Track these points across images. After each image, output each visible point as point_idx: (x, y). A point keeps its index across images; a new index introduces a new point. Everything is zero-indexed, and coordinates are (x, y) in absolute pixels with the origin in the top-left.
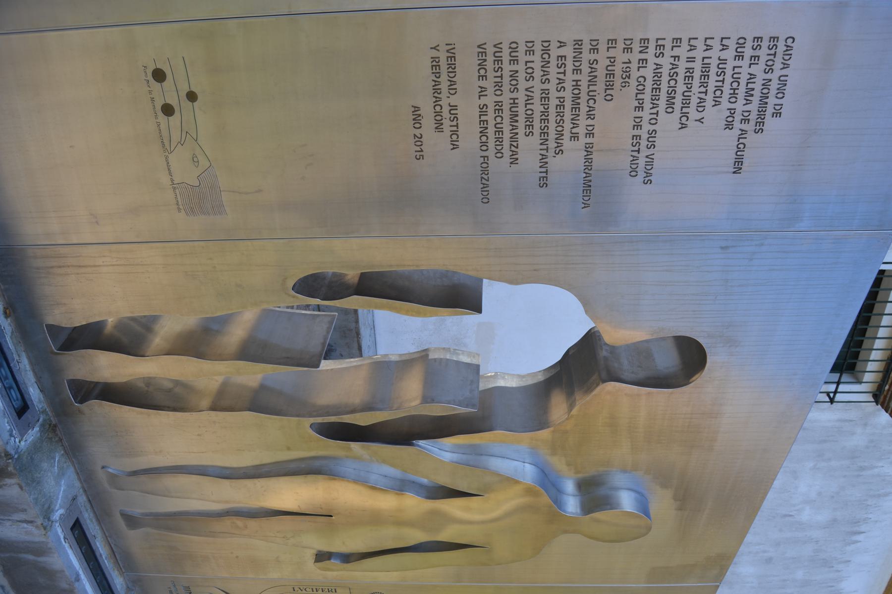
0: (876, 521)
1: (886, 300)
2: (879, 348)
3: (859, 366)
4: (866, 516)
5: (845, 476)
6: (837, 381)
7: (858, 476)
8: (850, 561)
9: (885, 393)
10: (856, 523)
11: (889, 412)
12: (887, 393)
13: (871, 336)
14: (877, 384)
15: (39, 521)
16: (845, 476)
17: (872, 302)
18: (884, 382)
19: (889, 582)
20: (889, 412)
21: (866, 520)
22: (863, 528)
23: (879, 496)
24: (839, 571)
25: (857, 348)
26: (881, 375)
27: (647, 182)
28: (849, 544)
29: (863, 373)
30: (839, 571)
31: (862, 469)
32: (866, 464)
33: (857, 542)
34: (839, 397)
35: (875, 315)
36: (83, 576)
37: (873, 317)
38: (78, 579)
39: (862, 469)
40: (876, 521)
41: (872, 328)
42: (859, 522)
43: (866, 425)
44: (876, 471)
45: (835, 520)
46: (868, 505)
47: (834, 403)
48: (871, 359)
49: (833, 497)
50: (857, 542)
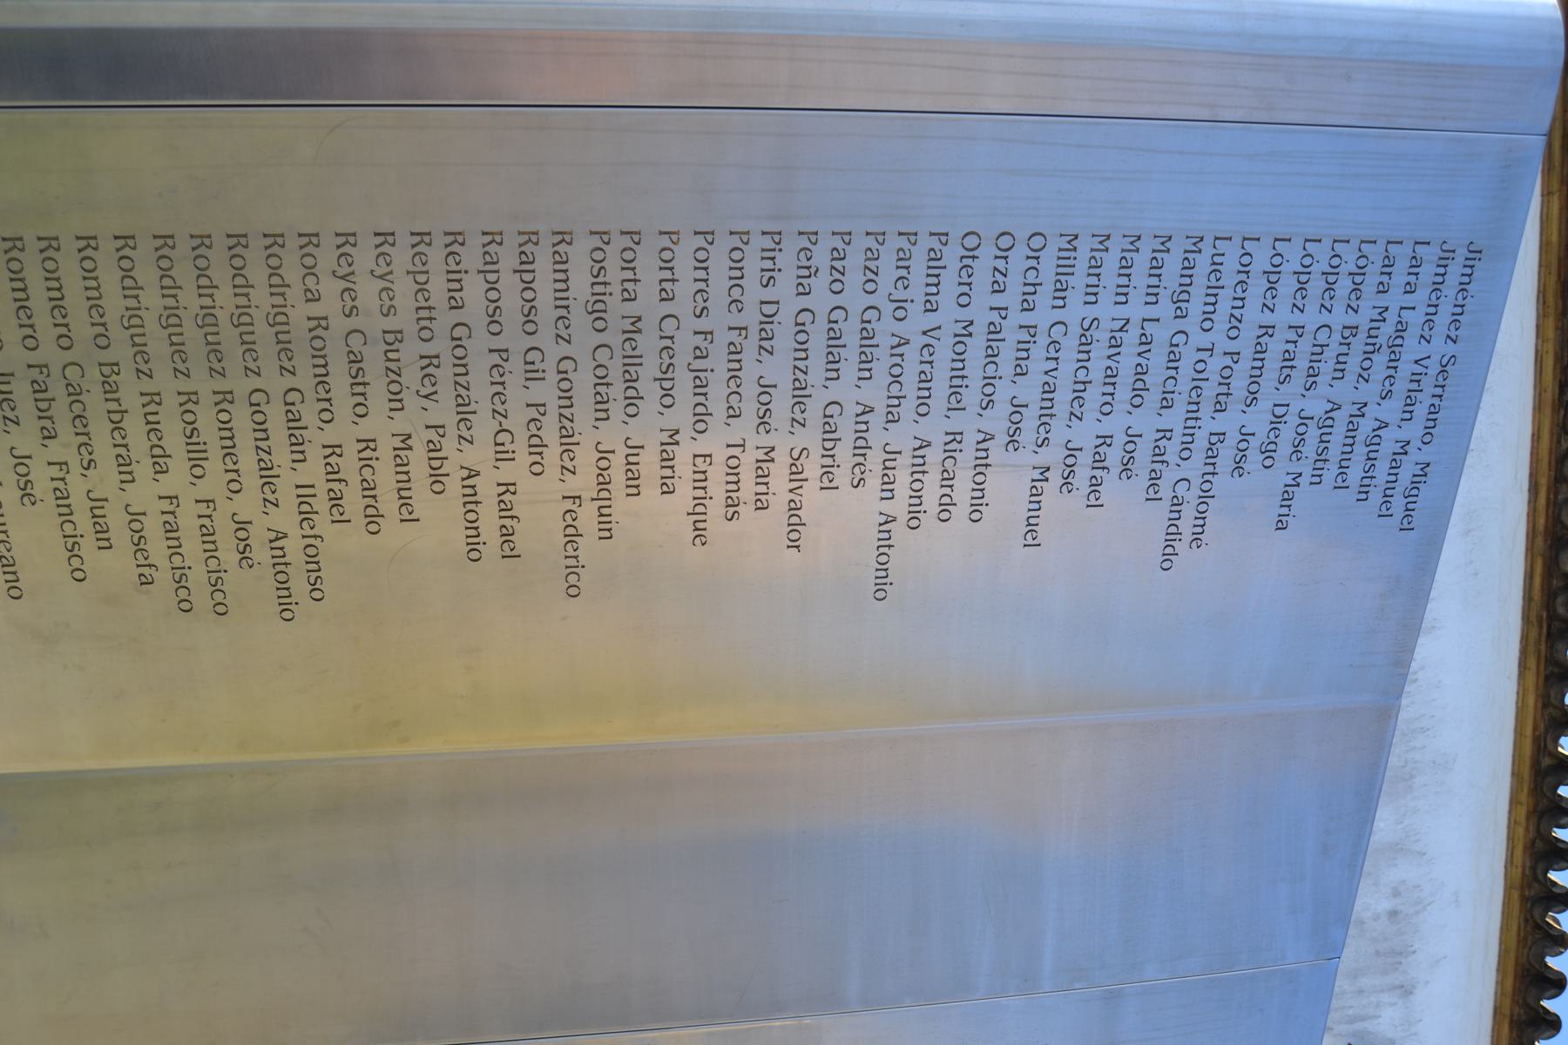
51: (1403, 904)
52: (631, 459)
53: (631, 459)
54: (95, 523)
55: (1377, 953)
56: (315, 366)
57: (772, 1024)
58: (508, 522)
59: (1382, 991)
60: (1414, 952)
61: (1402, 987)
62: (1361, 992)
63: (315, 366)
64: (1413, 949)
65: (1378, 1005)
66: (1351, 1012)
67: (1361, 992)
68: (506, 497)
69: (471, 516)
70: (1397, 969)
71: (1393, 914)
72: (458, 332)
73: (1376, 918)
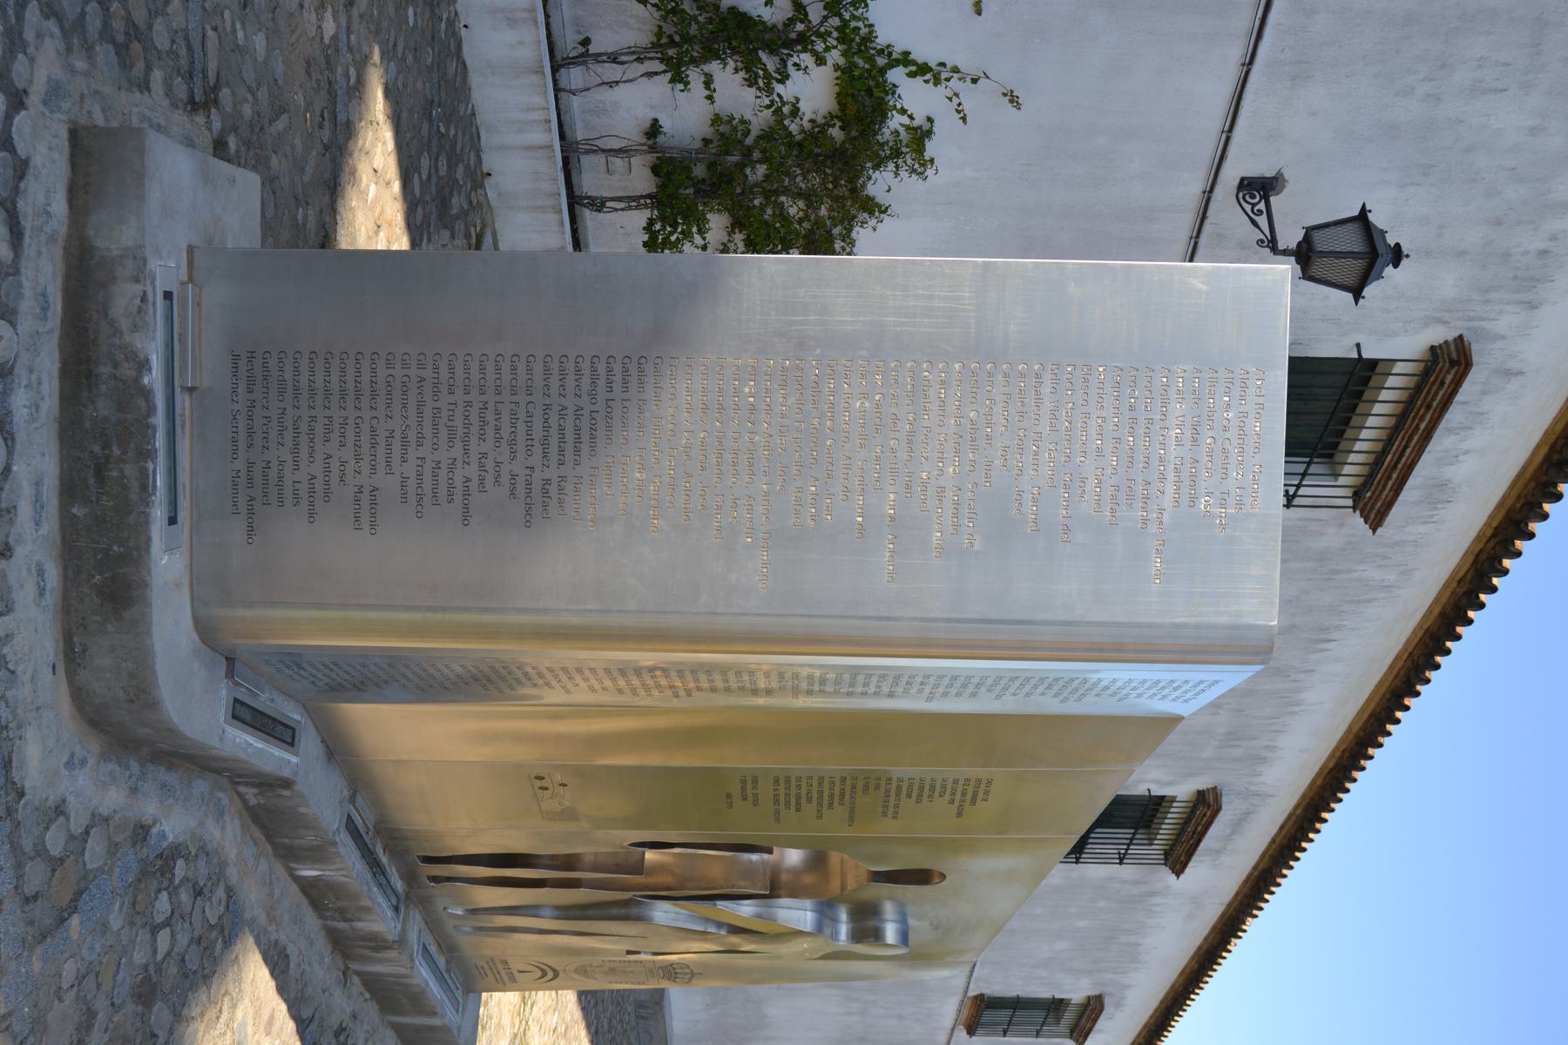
0: (1354, 629)
1: (1344, 461)
2: (1355, 462)
3: (1338, 457)
4: (1339, 623)
5: (1309, 580)
6: (1302, 471)
7: (1329, 580)
8: (1313, 671)
9: (1366, 500)
10: (1323, 630)
11: (1370, 522)
12: (1368, 502)
13: (1344, 449)
14: (1388, 431)
15: (409, 966)
16: (1309, 580)
17: (1366, 374)
18: (1365, 487)
19: (1371, 694)
20: (1370, 522)
21: (1338, 628)
22: (1334, 635)
23: (1359, 602)
24: (1298, 681)
25: (1332, 449)
26: (1421, 366)
27: (895, 817)
28: (1314, 652)
29: (1340, 466)
30: (1298, 681)
31: (1334, 572)
32: (1340, 567)
33: (1325, 650)
34: (1297, 501)
35: (1353, 427)
36: (430, 983)
37: (1354, 418)
38: (427, 985)
39: (1334, 572)
40: (1354, 629)
41: (1379, 376)
42: (1328, 629)
43: (1341, 525)
44: (1355, 575)
45: (1293, 627)
46: (1342, 612)
47: (1292, 508)
48: (1366, 425)
49: (1291, 601)
50: (1325, 650)
51: (1557, 246)
52: (404, 484)
53: (404, 484)
54: (624, 379)
55: (1516, 278)
56: (403, 399)
57: (370, 954)
58: (482, 473)
59: (1508, 303)
60: (1553, 281)
61: (1530, 303)
62: (1488, 301)
63: (403, 399)
64: (1552, 278)
65: (1500, 312)
66: (1472, 314)
67: (1488, 301)
68: (483, 460)
69: (373, 511)
70: (1529, 290)
71: (1544, 253)
72: (390, 379)
73: (1526, 253)
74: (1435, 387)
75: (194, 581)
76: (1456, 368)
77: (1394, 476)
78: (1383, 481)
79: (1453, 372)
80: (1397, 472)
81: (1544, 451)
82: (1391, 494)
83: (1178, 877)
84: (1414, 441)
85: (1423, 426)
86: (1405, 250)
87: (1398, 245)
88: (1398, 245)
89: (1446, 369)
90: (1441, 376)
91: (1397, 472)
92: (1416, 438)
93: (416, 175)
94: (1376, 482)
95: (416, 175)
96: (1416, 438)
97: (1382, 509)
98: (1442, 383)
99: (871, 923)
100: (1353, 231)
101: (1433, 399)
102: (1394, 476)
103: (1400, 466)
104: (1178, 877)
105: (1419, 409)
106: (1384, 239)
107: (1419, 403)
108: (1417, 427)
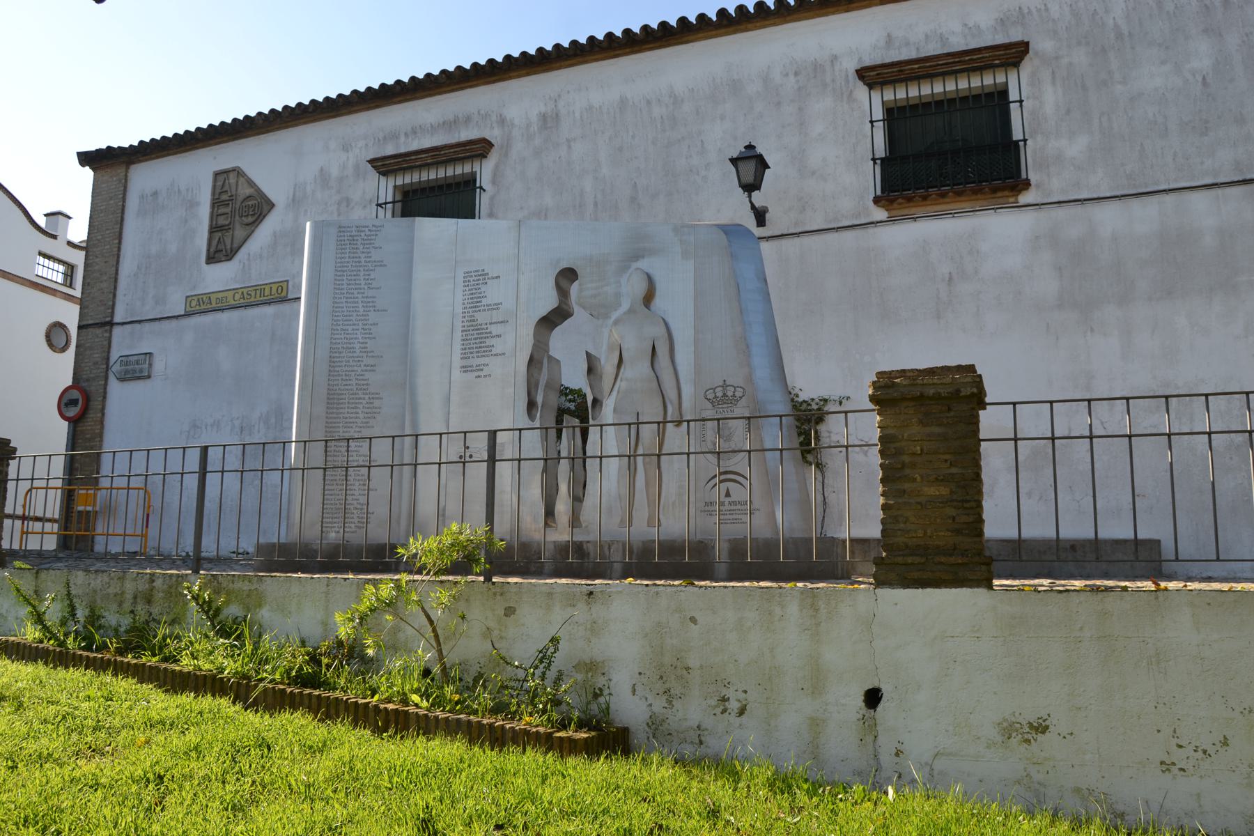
74: (885, 76)
75: (1018, 551)
76: (864, 74)
77: (967, 58)
78: (979, 61)
79: (868, 74)
80: (962, 59)
81: (788, 18)
82: (984, 52)
83: (769, 168)
84: (931, 64)
85: (916, 66)
86: (748, 144)
87: (745, 148)
88: (745, 148)
89: (868, 78)
90: (875, 77)
91: (962, 59)
92: (928, 64)
93: (28, 567)
94: (982, 64)
95: (28, 567)
96: (928, 64)
97: (1003, 49)
98: (878, 74)
99: (125, 666)
100: (741, 165)
101: (893, 72)
102: (967, 58)
103: (957, 60)
104: (769, 168)
105: (908, 74)
106: (743, 152)
107: (902, 76)
108: (918, 68)
